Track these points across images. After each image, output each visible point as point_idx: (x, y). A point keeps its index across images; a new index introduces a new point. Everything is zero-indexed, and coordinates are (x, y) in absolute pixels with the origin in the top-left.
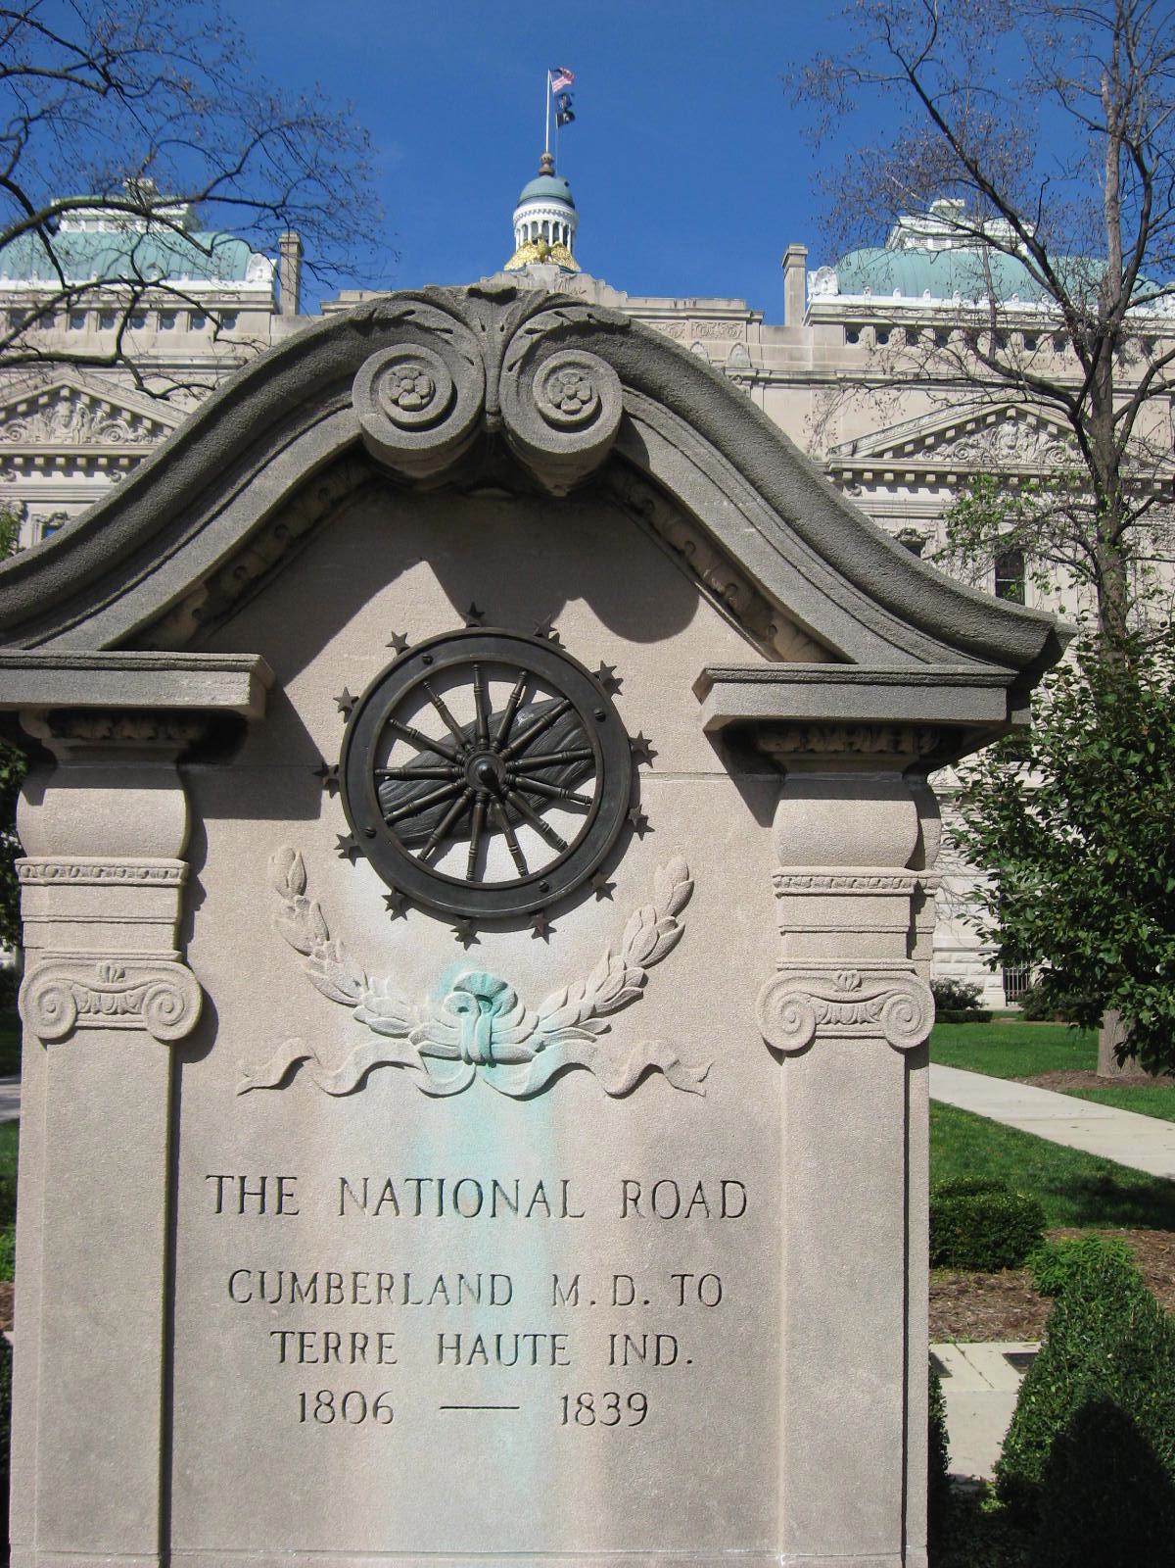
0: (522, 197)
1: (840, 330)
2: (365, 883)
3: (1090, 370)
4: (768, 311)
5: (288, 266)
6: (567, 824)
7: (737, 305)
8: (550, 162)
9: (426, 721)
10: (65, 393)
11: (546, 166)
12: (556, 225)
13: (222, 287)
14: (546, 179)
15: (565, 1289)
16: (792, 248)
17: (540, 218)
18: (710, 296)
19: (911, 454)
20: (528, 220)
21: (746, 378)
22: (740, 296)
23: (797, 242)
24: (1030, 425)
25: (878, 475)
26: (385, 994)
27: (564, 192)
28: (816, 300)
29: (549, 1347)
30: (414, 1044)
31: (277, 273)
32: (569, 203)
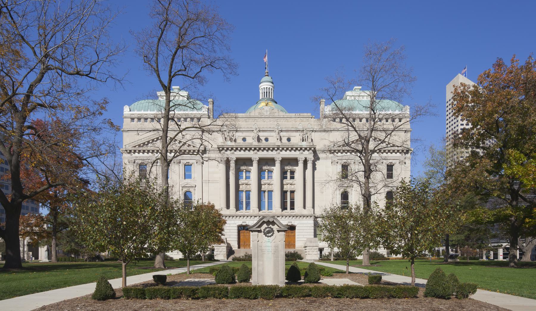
0: (261, 82)
2: (264, 236)
5: (211, 106)
6: (272, 234)
7: (309, 114)
8: (268, 73)
9: (266, 230)
11: (267, 74)
12: (269, 88)
13: (198, 113)
15: (272, 250)
17: (265, 87)
18: (303, 113)
20: (263, 87)
21: (311, 131)
22: (310, 113)
24: (373, 139)
26: (265, 240)
27: (271, 80)
29: (271, 251)
30: (286, 209)
31: (208, 109)
32: (273, 83)
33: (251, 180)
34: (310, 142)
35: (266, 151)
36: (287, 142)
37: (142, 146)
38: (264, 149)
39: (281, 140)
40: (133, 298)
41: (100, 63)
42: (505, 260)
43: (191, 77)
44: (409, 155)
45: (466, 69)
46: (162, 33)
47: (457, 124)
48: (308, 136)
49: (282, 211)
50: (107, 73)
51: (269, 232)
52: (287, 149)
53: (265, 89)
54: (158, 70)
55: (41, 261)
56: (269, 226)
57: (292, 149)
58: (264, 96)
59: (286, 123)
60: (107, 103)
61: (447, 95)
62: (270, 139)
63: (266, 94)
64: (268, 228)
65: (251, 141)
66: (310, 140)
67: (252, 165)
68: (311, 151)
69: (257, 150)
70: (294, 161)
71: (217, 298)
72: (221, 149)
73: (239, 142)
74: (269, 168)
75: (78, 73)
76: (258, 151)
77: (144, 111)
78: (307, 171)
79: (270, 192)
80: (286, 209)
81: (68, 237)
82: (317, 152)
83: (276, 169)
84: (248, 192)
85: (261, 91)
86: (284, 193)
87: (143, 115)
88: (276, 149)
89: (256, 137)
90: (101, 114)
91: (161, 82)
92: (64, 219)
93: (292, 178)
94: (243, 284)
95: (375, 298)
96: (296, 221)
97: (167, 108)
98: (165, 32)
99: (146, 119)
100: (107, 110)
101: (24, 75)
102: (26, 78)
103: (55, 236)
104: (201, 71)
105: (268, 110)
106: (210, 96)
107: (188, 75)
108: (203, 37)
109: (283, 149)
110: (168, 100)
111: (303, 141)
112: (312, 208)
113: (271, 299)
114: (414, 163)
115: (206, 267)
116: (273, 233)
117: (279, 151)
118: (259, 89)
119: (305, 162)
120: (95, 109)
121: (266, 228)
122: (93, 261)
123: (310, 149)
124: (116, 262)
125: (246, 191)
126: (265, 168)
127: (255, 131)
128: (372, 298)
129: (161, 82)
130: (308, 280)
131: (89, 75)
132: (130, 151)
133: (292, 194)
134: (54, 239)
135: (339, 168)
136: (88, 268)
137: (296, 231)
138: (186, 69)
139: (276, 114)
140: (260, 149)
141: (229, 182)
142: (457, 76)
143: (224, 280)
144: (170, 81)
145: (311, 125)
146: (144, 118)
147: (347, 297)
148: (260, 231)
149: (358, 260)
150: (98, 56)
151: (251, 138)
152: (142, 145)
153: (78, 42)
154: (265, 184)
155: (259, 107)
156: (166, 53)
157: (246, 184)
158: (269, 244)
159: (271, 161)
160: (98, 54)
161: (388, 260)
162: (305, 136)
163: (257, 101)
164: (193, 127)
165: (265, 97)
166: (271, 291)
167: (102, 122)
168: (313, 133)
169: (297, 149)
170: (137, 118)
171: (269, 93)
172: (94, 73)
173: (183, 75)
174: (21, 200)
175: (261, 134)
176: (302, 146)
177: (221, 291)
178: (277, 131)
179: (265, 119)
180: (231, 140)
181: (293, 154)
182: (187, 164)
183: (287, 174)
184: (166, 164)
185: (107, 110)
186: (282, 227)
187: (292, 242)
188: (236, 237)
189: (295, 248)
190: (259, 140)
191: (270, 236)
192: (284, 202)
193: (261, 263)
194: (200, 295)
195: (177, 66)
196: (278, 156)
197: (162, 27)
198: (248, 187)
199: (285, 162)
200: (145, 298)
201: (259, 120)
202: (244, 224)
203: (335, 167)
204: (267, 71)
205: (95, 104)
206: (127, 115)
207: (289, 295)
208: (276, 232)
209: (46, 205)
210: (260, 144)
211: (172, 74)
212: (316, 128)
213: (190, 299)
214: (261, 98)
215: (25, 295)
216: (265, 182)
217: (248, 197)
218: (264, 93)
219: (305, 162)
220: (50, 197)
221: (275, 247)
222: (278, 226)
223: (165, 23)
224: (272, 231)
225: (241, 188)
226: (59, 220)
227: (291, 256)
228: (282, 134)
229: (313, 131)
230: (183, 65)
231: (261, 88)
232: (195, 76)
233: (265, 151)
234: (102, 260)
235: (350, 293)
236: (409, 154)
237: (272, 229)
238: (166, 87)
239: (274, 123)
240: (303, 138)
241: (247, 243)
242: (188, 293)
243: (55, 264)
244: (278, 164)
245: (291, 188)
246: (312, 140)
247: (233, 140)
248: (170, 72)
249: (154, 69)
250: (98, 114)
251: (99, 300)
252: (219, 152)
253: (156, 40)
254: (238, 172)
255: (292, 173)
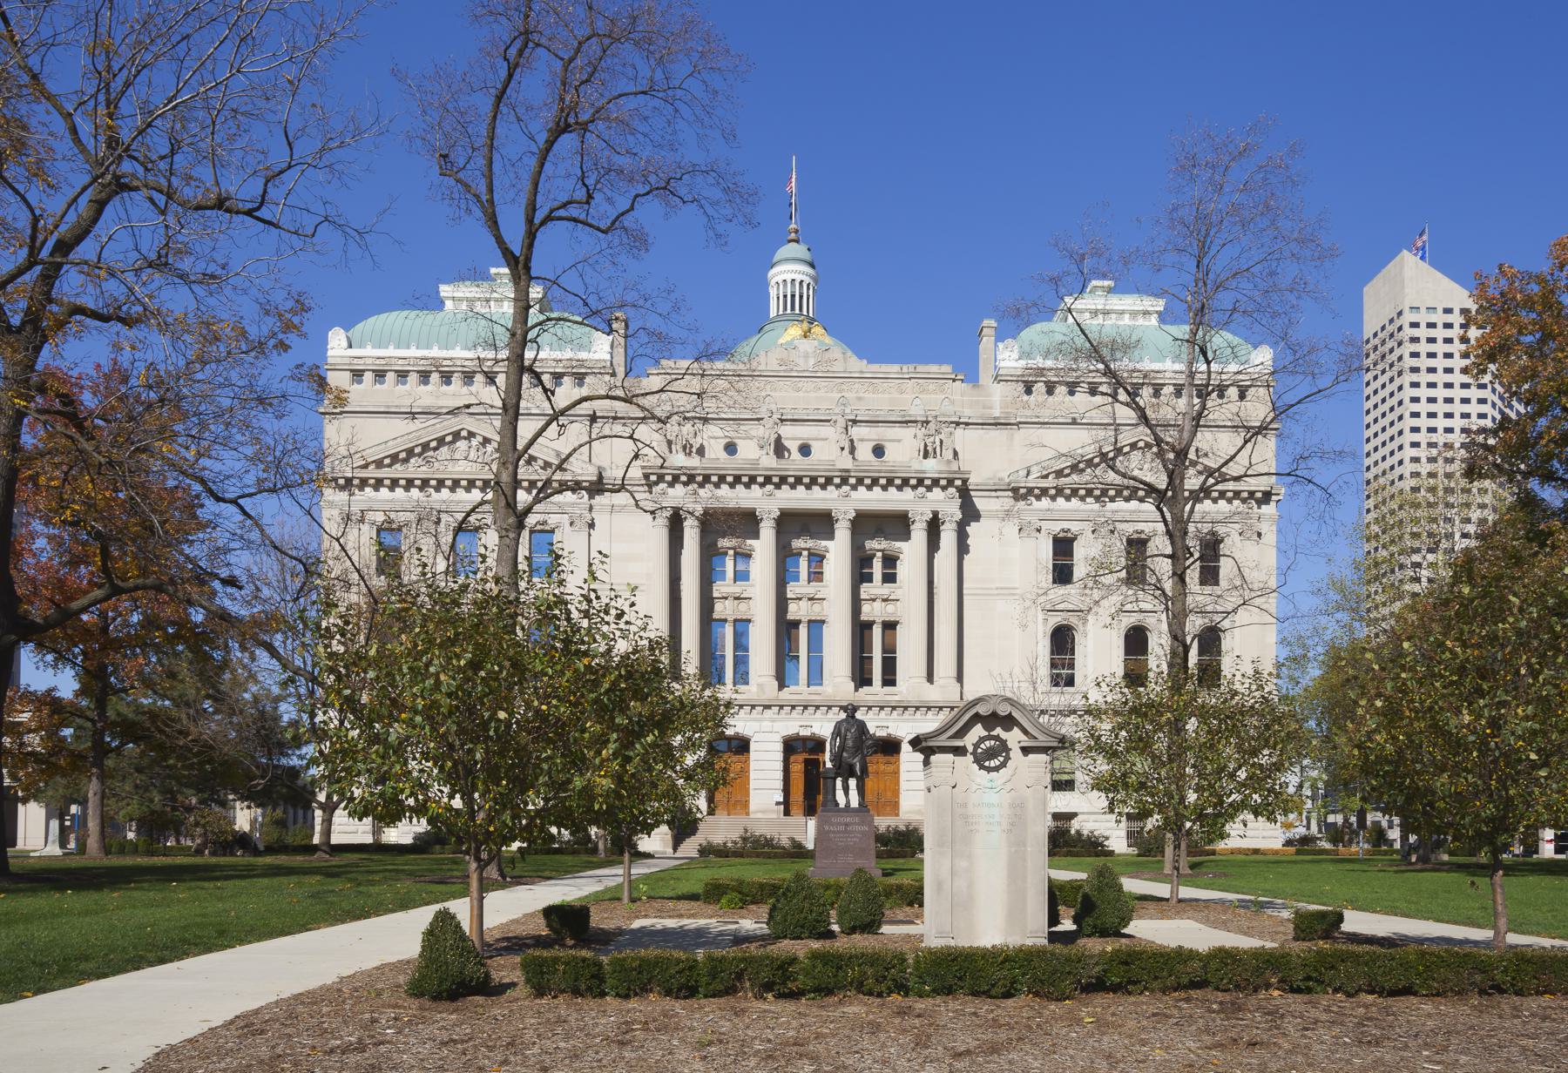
1: (1021, 387)
2: (975, 766)
3: (1171, 476)
4: (968, 371)
6: (1001, 759)
7: (947, 368)
8: (796, 231)
9: (982, 746)
10: (464, 433)
14: (793, 245)
16: (986, 322)
17: (789, 277)
19: (1068, 475)
20: (780, 278)
23: (990, 317)
25: (1044, 492)
27: (807, 256)
28: (1002, 364)
29: (999, 823)
30: (869, 682)
32: (812, 265)
33: (752, 586)
34: (949, 462)
35: (803, 487)
36: (871, 457)
37: (390, 466)
38: (799, 480)
39: (852, 450)
40: (563, 991)
41: (295, 173)
42: (1563, 857)
43: (598, 229)
44: (1269, 510)
45: (1425, 237)
46: (511, 76)
47: (1398, 412)
48: (941, 442)
49: (856, 690)
50: (318, 208)
51: (991, 754)
52: (875, 481)
53: (789, 285)
54: (491, 201)
55: (37, 854)
56: (994, 733)
57: (890, 482)
58: (785, 309)
59: (871, 395)
60: (306, 309)
61: (1366, 318)
62: (816, 447)
63: (791, 300)
64: (989, 738)
65: (753, 454)
66: (949, 455)
67: (756, 536)
68: (952, 490)
69: (775, 484)
70: (898, 524)
71: (870, 994)
72: (653, 478)
73: (713, 456)
74: (810, 543)
75: (220, 204)
76: (778, 486)
77: (397, 347)
78: (938, 556)
79: (816, 625)
80: (869, 682)
81: (139, 770)
82: (972, 493)
83: (838, 551)
84: (741, 626)
85: (773, 292)
86: (861, 629)
87: (393, 361)
88: (837, 481)
89: (772, 440)
90: (283, 347)
91: (499, 240)
92: (124, 709)
93: (890, 578)
94: (861, 942)
95: (1438, 995)
96: (901, 724)
97: (519, 332)
98: (516, 77)
99: (380, 375)
100: (304, 336)
101: (71, 196)
102: (73, 207)
103: (100, 766)
104: (632, 208)
105: (810, 351)
106: (665, 295)
107: (590, 221)
108: (644, 93)
109: (860, 481)
110: (520, 304)
111: (926, 456)
112: (954, 681)
113: (1068, 998)
114: (1330, 530)
115: (570, 872)
116: (1008, 758)
117: (846, 488)
118: (766, 284)
119: (934, 526)
120: (265, 331)
121: (982, 740)
122: (225, 855)
123: (950, 482)
124: (312, 858)
125: (736, 621)
126: (798, 543)
127: (769, 423)
128: (1426, 996)
129: (499, 240)
130: (1095, 927)
131: (256, 214)
132: (349, 481)
133: (887, 632)
134: (94, 779)
135: (1046, 549)
136: (227, 878)
137: (753, 755)
138: (590, 197)
139: (838, 367)
140: (783, 480)
141: (679, 591)
142: (1398, 258)
143: (803, 927)
144: (531, 236)
145: (953, 402)
146: (396, 371)
147: (1336, 991)
148: (959, 751)
149: (1119, 855)
150: (291, 149)
151: (753, 444)
152: (387, 461)
153: (226, 98)
154: (800, 599)
155: (782, 341)
156: (516, 144)
157: (736, 598)
158: (992, 797)
159: (820, 523)
160: (291, 139)
161: (1212, 857)
162: (932, 439)
163: (760, 322)
164: (608, 397)
165: (789, 311)
166: (1068, 969)
167: (289, 374)
168: (959, 431)
169: (906, 482)
170: (374, 371)
171: (801, 297)
172: (272, 207)
173: (575, 220)
174: (13, 637)
175: (787, 431)
176: (924, 472)
177: (887, 969)
178: (841, 423)
179: (802, 383)
180: (687, 449)
181: (894, 498)
182: (539, 527)
183: (871, 567)
184: (512, 520)
185: (304, 336)
186: (1041, 737)
187: (889, 794)
188: (779, 775)
189: (897, 815)
190: (780, 449)
191: (997, 769)
192: (862, 658)
193: (962, 864)
194: (801, 981)
195: (559, 185)
196: (844, 504)
197: (513, 52)
198: (743, 606)
199: (868, 524)
200: (603, 994)
201: (781, 383)
202: (805, 733)
203: (1031, 543)
204: (793, 226)
205: (267, 313)
206: (339, 361)
207: (1130, 982)
208: (1016, 753)
209: (68, 659)
210: (783, 464)
211: (537, 221)
212: (968, 413)
213: (770, 996)
214: (773, 313)
215: (114, 975)
216: (798, 590)
217: (741, 645)
218: (785, 296)
219: (934, 526)
220: (86, 633)
221: (1013, 806)
222: (1025, 732)
223: (518, 44)
224: (1003, 748)
225: (720, 609)
226: (111, 714)
227: (897, 840)
228: (856, 432)
229: (958, 424)
230: (584, 184)
231: (773, 282)
232: (613, 223)
233: (801, 488)
234: (256, 852)
235: (1350, 978)
236: (1273, 504)
237: (1004, 743)
238: (516, 259)
239: (829, 395)
240: (926, 446)
241: (739, 798)
242: (765, 976)
243: (98, 863)
244: (843, 533)
245: (815, 611)
246: (956, 453)
247: (694, 450)
248: (532, 208)
249: (477, 196)
250: (275, 346)
251: (436, 998)
252: (646, 488)
253: (485, 103)
254: (710, 555)
255: (890, 561)
